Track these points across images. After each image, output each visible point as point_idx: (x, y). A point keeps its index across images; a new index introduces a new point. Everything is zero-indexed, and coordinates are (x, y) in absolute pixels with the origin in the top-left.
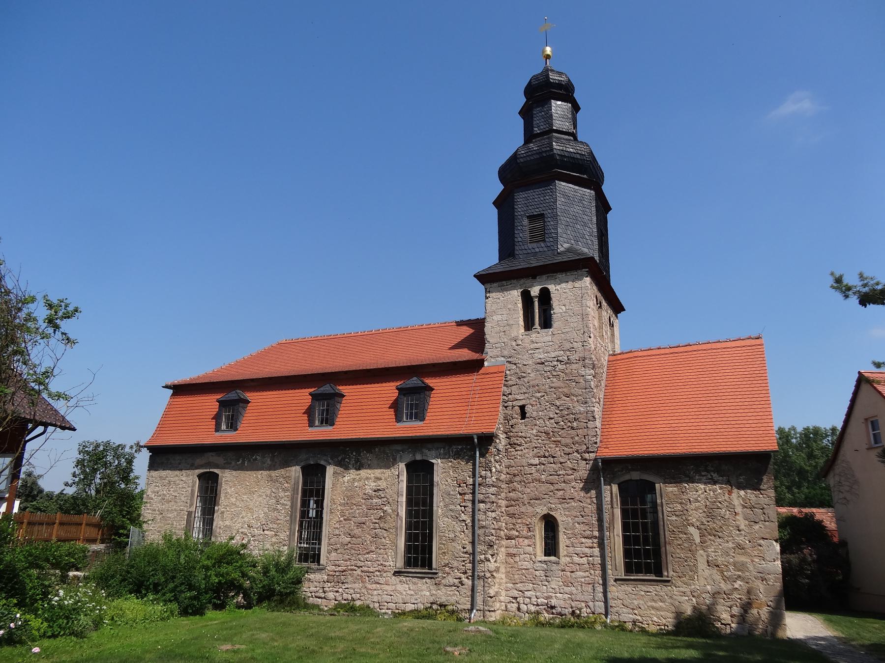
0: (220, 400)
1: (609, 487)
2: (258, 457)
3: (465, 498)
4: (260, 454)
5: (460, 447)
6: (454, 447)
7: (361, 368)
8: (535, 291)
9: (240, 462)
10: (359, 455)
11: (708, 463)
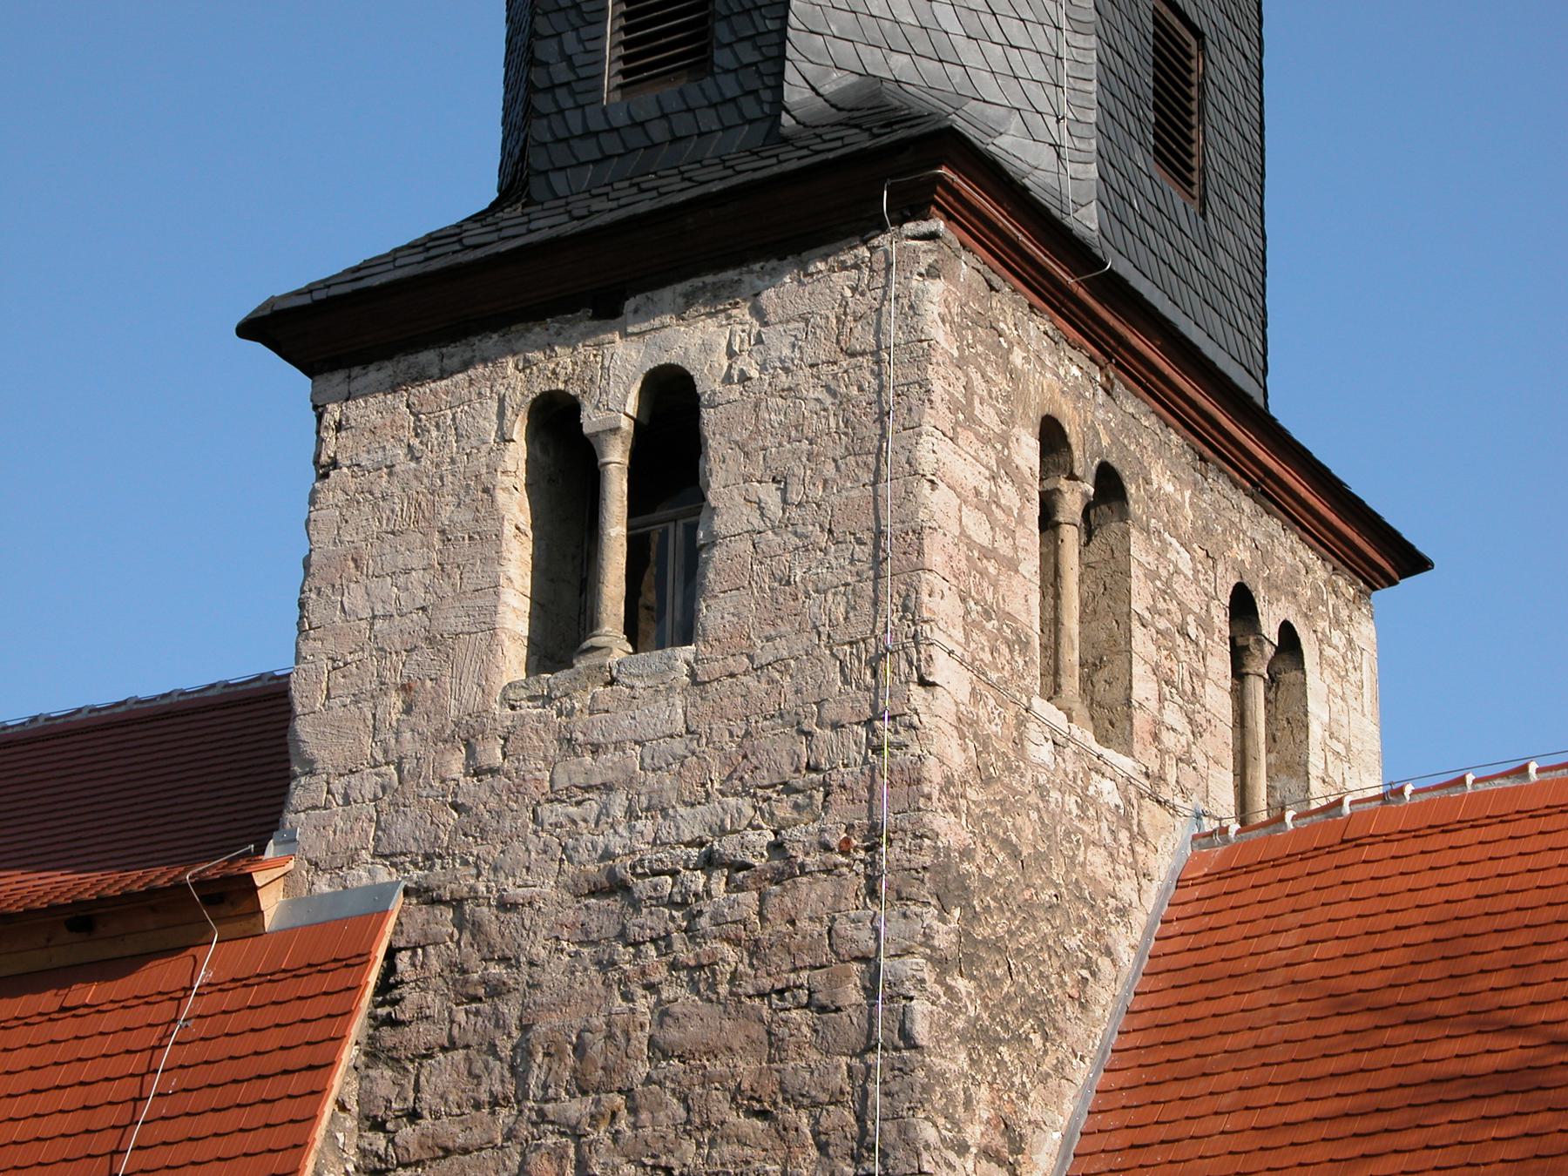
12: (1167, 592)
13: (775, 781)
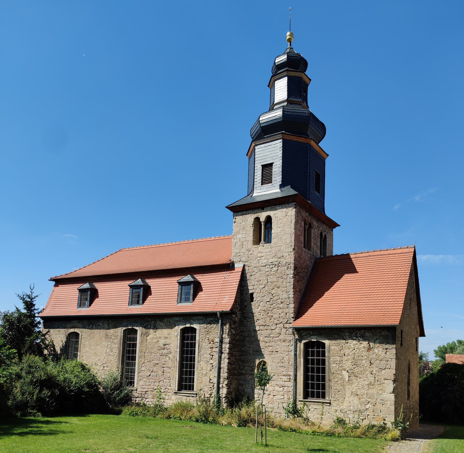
0: (79, 288)
2: (100, 323)
3: (213, 350)
4: (102, 322)
5: (211, 319)
6: (208, 319)
7: (160, 269)
8: (263, 219)
10: (156, 323)
12: (315, 235)
13: (331, 353)
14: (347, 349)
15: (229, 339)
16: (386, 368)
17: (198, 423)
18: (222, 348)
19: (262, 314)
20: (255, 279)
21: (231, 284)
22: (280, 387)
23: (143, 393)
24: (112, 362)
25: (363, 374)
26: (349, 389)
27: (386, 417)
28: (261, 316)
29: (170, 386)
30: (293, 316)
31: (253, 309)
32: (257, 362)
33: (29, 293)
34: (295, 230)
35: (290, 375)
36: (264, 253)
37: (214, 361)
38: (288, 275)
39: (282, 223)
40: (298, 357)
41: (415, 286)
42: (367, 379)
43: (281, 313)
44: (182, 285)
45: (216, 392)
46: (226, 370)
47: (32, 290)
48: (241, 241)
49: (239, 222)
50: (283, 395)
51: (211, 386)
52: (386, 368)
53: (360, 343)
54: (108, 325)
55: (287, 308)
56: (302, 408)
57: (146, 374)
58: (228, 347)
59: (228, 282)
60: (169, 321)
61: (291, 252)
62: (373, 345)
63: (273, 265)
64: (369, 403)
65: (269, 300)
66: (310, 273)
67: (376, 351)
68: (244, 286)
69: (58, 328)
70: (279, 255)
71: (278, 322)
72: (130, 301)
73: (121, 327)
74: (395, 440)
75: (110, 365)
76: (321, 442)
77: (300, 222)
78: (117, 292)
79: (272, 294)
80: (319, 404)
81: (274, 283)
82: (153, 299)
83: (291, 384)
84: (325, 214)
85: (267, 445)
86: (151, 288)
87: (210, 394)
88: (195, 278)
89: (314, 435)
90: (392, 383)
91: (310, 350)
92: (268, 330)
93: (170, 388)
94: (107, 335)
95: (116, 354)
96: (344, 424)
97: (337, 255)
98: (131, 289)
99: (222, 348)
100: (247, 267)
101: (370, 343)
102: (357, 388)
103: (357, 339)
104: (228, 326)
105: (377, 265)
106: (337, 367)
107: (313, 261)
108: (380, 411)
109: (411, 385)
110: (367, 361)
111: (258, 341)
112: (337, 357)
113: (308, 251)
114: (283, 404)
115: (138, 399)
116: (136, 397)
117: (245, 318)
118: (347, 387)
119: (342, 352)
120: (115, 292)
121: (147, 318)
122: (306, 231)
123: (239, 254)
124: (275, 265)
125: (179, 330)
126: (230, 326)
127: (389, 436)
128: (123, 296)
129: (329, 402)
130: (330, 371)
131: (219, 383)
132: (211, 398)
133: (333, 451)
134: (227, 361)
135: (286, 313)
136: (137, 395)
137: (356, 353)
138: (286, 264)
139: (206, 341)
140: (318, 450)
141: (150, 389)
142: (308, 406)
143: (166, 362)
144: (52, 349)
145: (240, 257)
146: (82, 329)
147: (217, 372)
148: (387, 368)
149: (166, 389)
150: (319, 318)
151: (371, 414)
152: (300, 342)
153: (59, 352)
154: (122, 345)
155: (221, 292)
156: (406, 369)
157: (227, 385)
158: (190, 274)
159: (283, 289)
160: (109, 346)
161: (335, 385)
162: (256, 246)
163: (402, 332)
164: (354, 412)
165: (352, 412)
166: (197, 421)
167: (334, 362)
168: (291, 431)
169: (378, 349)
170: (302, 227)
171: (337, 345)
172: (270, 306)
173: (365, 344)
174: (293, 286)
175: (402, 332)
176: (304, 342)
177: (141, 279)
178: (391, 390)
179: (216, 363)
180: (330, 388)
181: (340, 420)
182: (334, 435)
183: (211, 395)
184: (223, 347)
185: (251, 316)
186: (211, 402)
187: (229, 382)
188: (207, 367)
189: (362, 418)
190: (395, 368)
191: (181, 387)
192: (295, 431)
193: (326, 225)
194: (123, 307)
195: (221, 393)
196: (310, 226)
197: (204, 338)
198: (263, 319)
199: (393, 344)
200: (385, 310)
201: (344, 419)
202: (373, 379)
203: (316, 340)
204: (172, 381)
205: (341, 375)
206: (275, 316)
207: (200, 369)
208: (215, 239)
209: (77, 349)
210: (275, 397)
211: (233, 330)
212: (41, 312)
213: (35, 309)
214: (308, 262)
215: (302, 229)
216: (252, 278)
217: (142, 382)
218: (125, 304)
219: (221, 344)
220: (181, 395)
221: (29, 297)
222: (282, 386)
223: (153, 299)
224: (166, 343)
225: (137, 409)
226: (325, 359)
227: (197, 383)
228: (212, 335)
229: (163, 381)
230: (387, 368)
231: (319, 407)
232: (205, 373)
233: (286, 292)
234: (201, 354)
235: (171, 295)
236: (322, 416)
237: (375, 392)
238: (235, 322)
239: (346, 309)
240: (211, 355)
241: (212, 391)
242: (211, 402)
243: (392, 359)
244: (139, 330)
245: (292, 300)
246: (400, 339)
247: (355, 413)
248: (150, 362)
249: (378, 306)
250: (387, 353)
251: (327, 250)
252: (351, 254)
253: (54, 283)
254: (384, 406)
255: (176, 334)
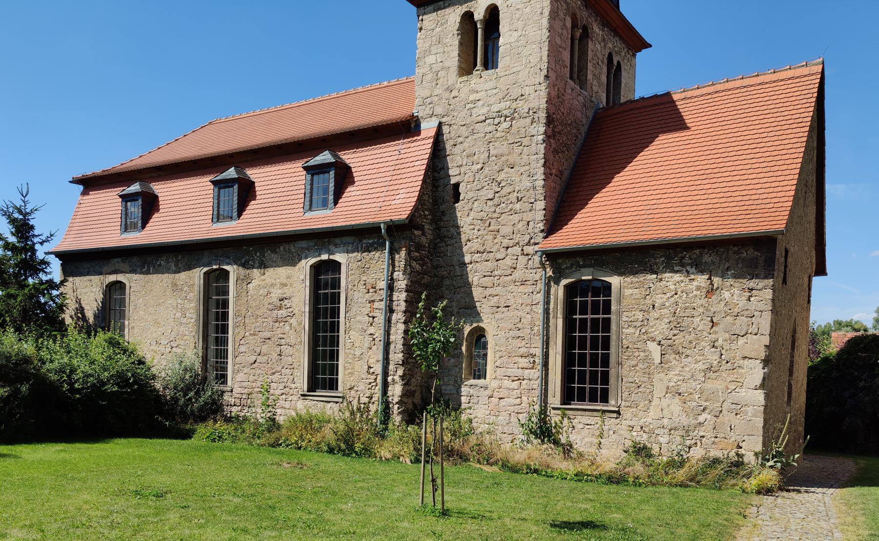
1: (470, 266)
2: (162, 262)
4: (164, 259)
5: (371, 242)
6: (365, 241)
9: (146, 268)
10: (264, 256)
11: (684, 253)
13: (624, 303)
14: (660, 294)
15: (405, 282)
16: (747, 333)
17: (331, 455)
18: (393, 301)
19: (477, 228)
20: (464, 151)
21: (412, 165)
22: (513, 381)
23: (244, 397)
24: (185, 337)
25: (695, 348)
26: (661, 382)
27: (744, 441)
28: (476, 231)
29: (293, 382)
30: (542, 228)
31: (459, 218)
32: (467, 329)
33: (19, 203)
34: (549, 31)
35: (533, 356)
36: (482, 93)
37: (376, 328)
38: (533, 136)
39: (521, 19)
40: (551, 316)
41: (815, 159)
42: (702, 357)
43: (516, 222)
44: (313, 172)
45: (380, 392)
46: (400, 347)
47: (24, 197)
48: (434, 70)
49: (429, 28)
50: (520, 396)
51: (372, 381)
52: (747, 333)
53: (690, 278)
54: (176, 265)
55: (531, 210)
56: (558, 422)
57: (248, 359)
58: (405, 299)
59: (407, 160)
60: (289, 249)
61: (540, 84)
62: (720, 283)
63: (501, 116)
64: (707, 412)
65: (491, 197)
66: (583, 138)
67: (726, 295)
68: (440, 169)
69: (88, 274)
70: (515, 93)
71: (511, 243)
72: (215, 213)
73: (200, 267)
74: (765, 491)
75: (182, 343)
76: (591, 500)
77: (563, 17)
78: (193, 198)
79: (499, 181)
80: (595, 414)
81: (503, 158)
82: (258, 206)
83: (536, 373)
84: (619, 10)
85: (445, 513)
86: (256, 185)
87: (368, 397)
88: (340, 158)
89: (579, 480)
90: (761, 365)
91: (578, 299)
92: (490, 261)
93: (293, 386)
94: (176, 285)
95: (193, 320)
96: (650, 456)
97: (643, 99)
98: (216, 190)
99: (391, 301)
100: (446, 127)
101: (712, 278)
102: (680, 378)
103: (684, 271)
104: (403, 253)
105: (733, 109)
106: (637, 334)
107: (591, 114)
108: (729, 429)
109: (795, 375)
110: (705, 318)
111: (469, 285)
112: (637, 313)
113: (578, 88)
114: (519, 415)
115: (235, 409)
116: (231, 405)
117: (442, 238)
118: (656, 377)
119: (649, 301)
120: (189, 199)
121: (246, 246)
122: (577, 42)
123: (429, 100)
124: (506, 117)
125: (308, 268)
126: (409, 253)
127: (753, 483)
128: (203, 205)
129: (617, 409)
130: (620, 344)
131: (385, 374)
132: (370, 405)
133: (620, 526)
134: (401, 327)
135: (528, 222)
136: (233, 400)
137: (681, 301)
138: (528, 113)
139: (361, 287)
140: (579, 523)
141: (256, 389)
142: (570, 419)
143: (284, 334)
144: (79, 315)
145: (431, 105)
146: (131, 275)
147: (382, 351)
148: (749, 332)
149: (285, 387)
150: (600, 229)
151: (710, 434)
152: (557, 283)
153: (91, 320)
154: (202, 302)
155: (391, 183)
156: (788, 338)
157: (402, 377)
158: (329, 150)
159: (522, 170)
160: (179, 306)
161: (630, 374)
162: (465, 78)
163: (787, 251)
164: (670, 430)
165: (666, 431)
166: (331, 451)
167: (630, 324)
168: (527, 473)
169: (732, 291)
170: (566, 29)
171: (637, 285)
172: (493, 210)
173: (701, 280)
174: (543, 160)
175: (787, 251)
176: (564, 282)
177: (236, 167)
178: (758, 381)
179: (379, 334)
180: (620, 380)
181: (640, 447)
182: (624, 481)
183: (372, 398)
184: (395, 298)
185: (455, 234)
186: (371, 413)
187: (407, 372)
188: (362, 342)
189: (688, 443)
190: (768, 332)
191: (313, 385)
192: (536, 471)
193: (622, 38)
194: (202, 226)
195: (390, 393)
196: (586, 34)
197: (356, 283)
198: (480, 237)
199: (766, 277)
200: (751, 202)
201: (649, 446)
202: (717, 358)
203: (590, 277)
204: (297, 372)
205: (644, 351)
206: (505, 230)
207: (348, 345)
208: (389, 84)
209: (122, 315)
210: (503, 402)
211: (414, 262)
212: (47, 241)
213: (34, 236)
214: (579, 114)
215: (567, 34)
216: (457, 150)
217: (241, 374)
218: (206, 222)
219: (390, 292)
220: (314, 400)
221: (20, 211)
222: (517, 378)
223: (258, 206)
224: (284, 296)
225: (225, 427)
226: (610, 318)
227: (345, 374)
228: (373, 275)
229: (279, 372)
230: (751, 333)
231: (596, 420)
232: (360, 353)
233: (529, 176)
234: (352, 315)
235: (293, 197)
236: (601, 440)
237: (720, 386)
238: (419, 247)
239: (660, 206)
240: (370, 317)
241: (373, 391)
242: (371, 413)
243: (764, 313)
244: (233, 270)
245: (540, 192)
246: (783, 268)
247: (672, 432)
248: (254, 335)
249: (734, 194)
250: (752, 299)
251: (622, 97)
252: (675, 93)
253: (81, 188)
254: (738, 416)
255: (302, 277)
